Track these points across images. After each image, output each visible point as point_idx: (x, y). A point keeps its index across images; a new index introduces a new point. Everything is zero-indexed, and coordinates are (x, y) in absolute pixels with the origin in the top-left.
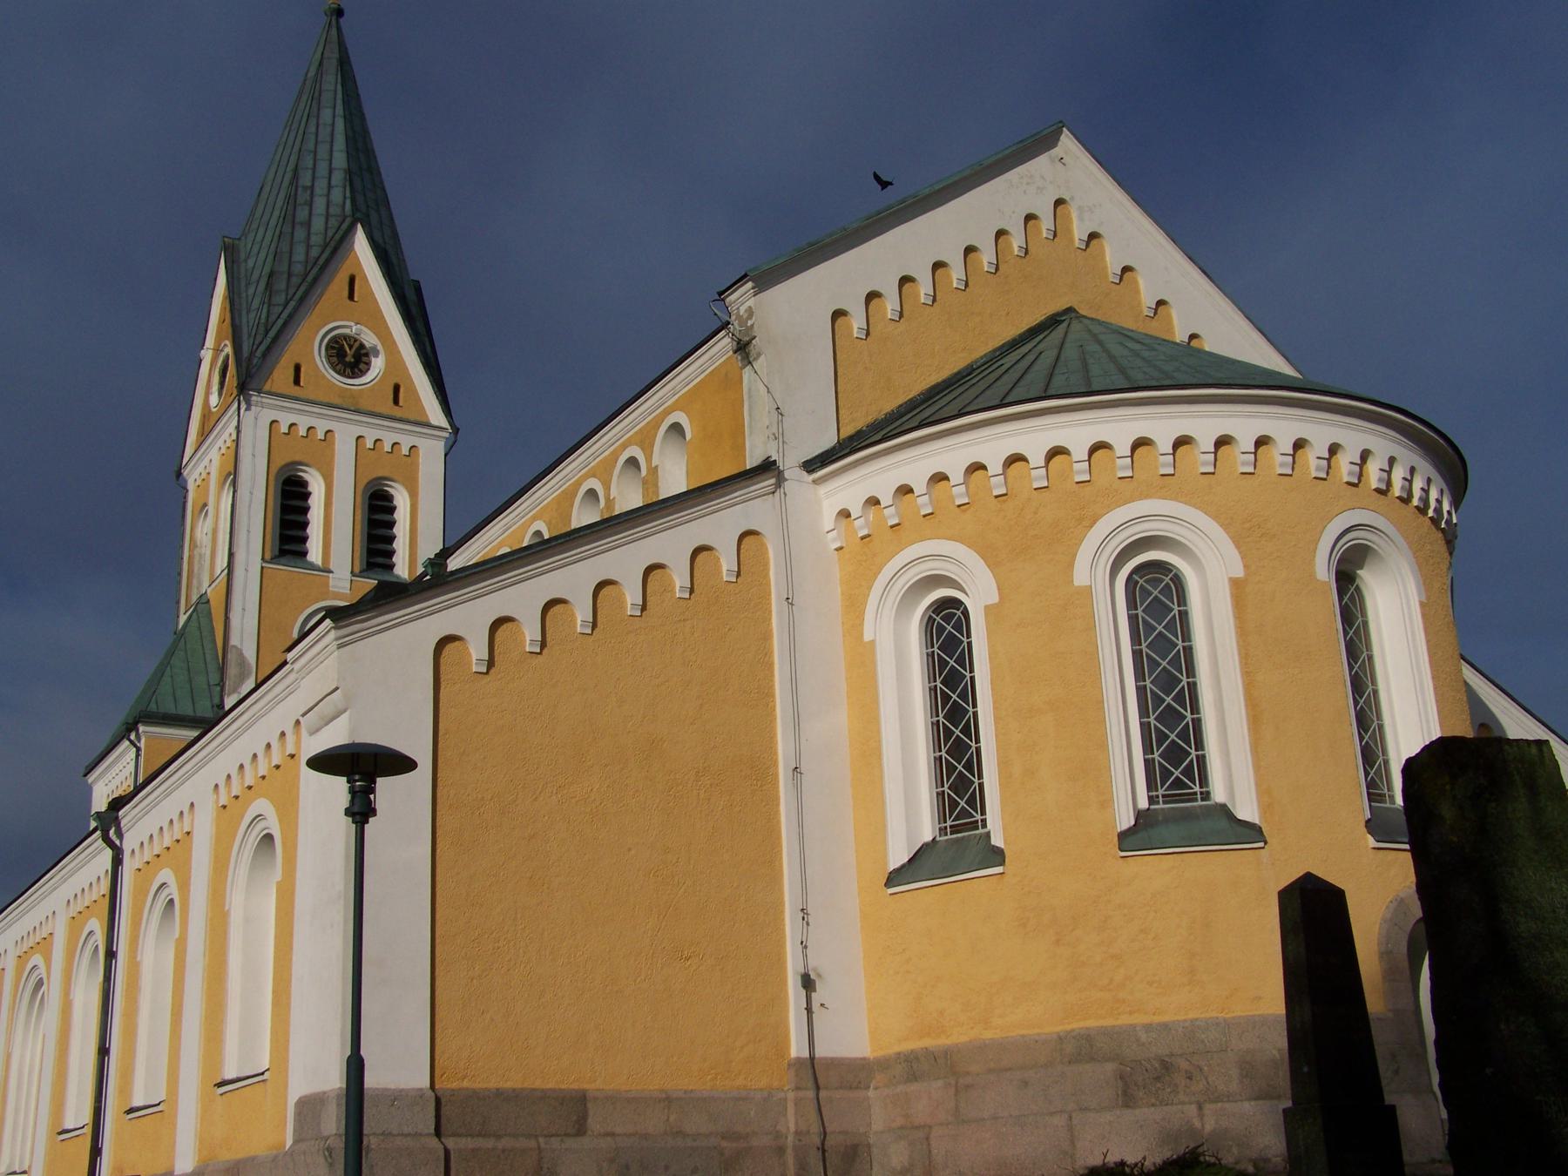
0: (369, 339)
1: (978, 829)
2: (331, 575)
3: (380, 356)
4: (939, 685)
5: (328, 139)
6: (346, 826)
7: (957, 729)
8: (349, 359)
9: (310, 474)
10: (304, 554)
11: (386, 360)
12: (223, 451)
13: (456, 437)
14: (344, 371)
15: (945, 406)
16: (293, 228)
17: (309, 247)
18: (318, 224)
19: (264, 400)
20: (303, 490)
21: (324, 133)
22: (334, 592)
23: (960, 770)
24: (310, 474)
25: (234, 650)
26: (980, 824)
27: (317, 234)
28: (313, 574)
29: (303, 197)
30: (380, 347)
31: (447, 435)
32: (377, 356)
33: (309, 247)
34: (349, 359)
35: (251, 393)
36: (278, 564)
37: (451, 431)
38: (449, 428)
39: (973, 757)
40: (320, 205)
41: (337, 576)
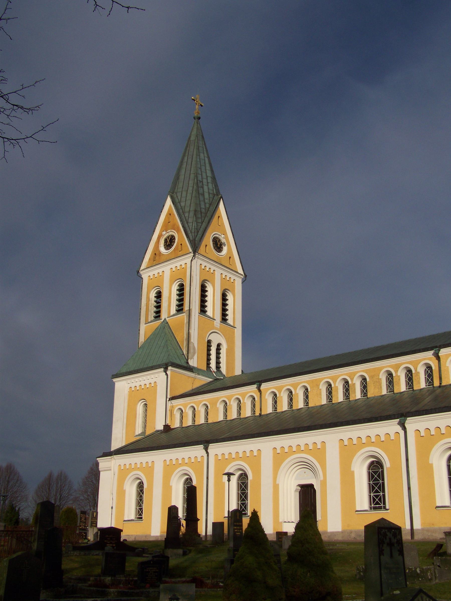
0: (223, 240)
1: (382, 509)
2: (215, 321)
3: (226, 246)
4: (362, 388)
5: (204, 165)
6: (111, 509)
7: (376, 489)
8: (219, 246)
9: (208, 284)
10: (206, 311)
11: (228, 248)
12: (174, 270)
13: (246, 279)
14: (215, 247)
15: (183, 185)
16: (199, 195)
17: (205, 203)
18: (206, 196)
19: (199, 256)
20: (204, 289)
21: (202, 162)
22: (216, 327)
23: (377, 501)
24: (208, 284)
25: (192, 343)
26: (383, 507)
27: (207, 199)
28: (211, 320)
29: (200, 184)
30: (226, 243)
31: (243, 277)
32: (225, 246)
33: (205, 203)
34: (219, 246)
35: (196, 253)
36: (202, 315)
37: (244, 276)
38: (244, 275)
39: (381, 484)
40: (205, 188)
41: (217, 322)
